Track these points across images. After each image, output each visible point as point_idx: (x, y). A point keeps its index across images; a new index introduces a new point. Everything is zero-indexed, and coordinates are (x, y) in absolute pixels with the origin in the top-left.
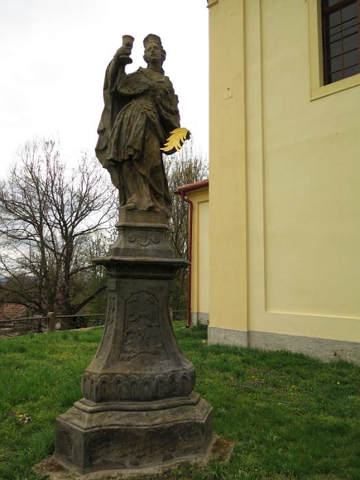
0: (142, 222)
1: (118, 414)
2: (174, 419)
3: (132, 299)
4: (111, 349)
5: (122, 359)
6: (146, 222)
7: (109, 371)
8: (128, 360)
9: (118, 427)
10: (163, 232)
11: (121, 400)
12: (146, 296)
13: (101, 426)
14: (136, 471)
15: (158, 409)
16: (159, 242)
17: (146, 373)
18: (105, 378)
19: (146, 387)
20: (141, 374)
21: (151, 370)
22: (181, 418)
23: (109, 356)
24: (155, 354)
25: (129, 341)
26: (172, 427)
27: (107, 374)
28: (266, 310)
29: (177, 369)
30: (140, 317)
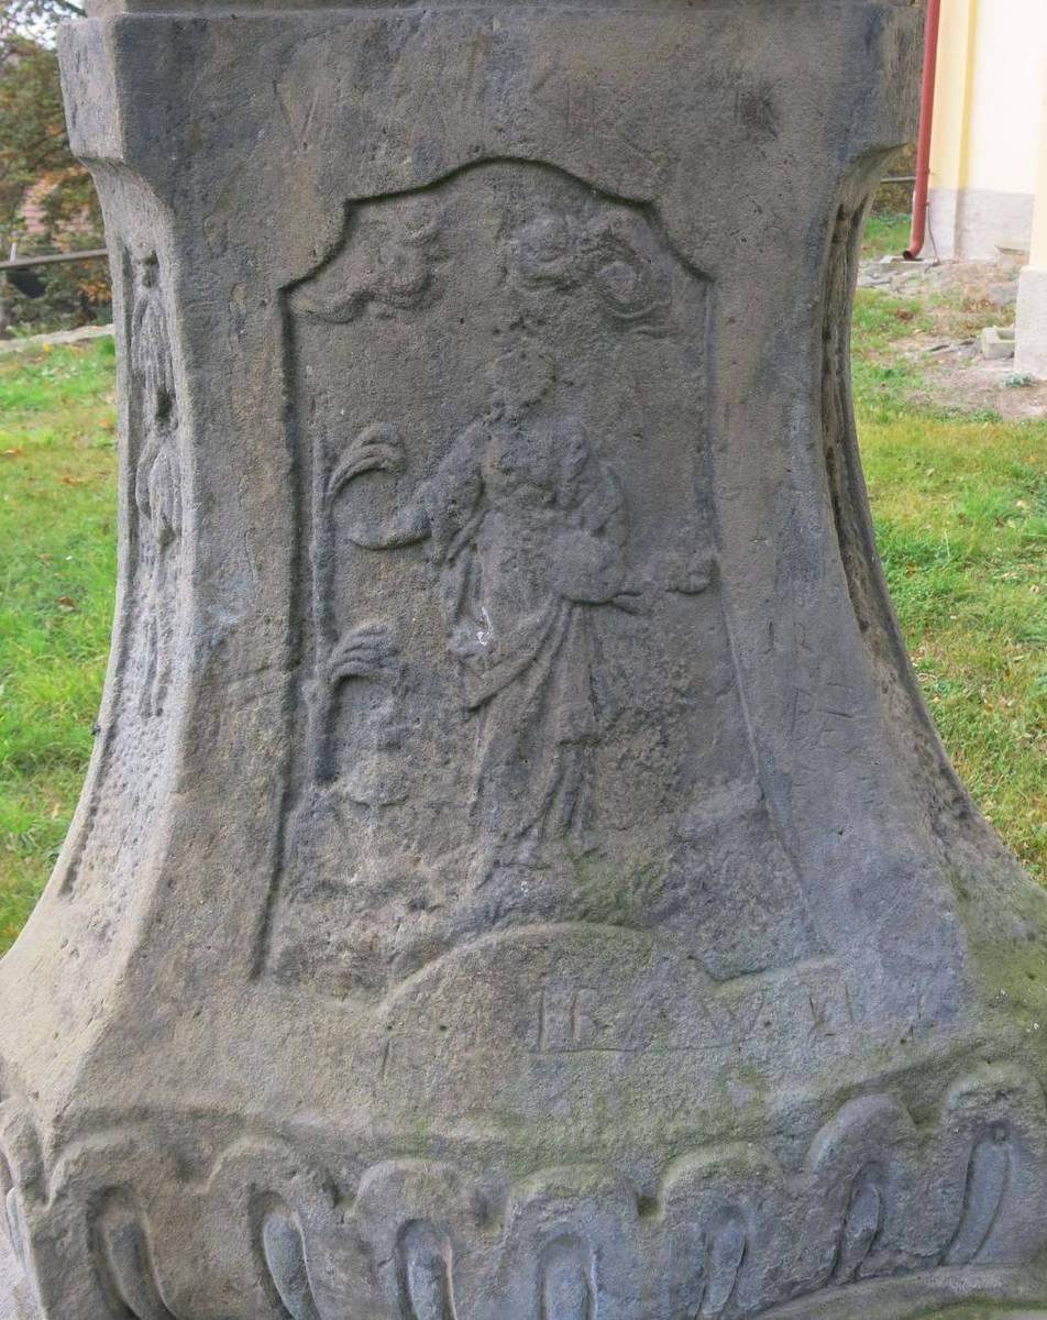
3: (354, 272)
4: (174, 852)
5: (297, 966)
12: (543, 225)
23: (155, 921)
25: (361, 777)
30: (477, 496)
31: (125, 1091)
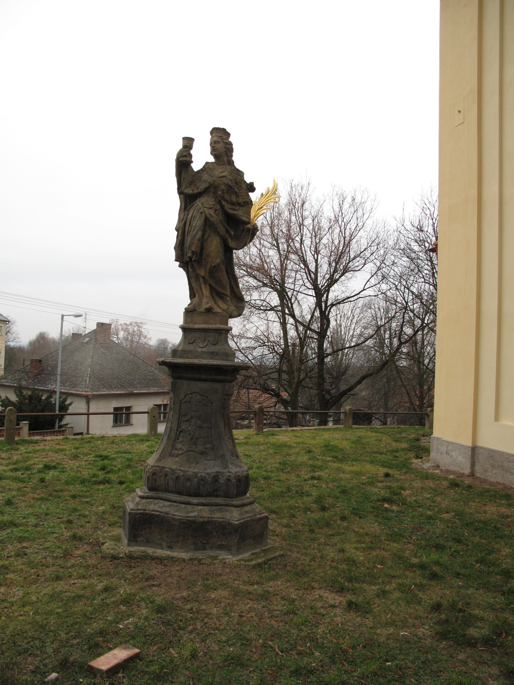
0: (200, 324)
1: (162, 503)
2: (210, 516)
3: (185, 400)
5: (173, 456)
6: (205, 323)
7: (160, 464)
8: (177, 456)
9: (158, 513)
10: (221, 333)
11: (170, 492)
13: (145, 510)
14: (169, 553)
15: (198, 505)
16: (217, 343)
17: (190, 470)
18: (156, 469)
19: (188, 483)
20: (184, 470)
21: (195, 468)
22: (218, 516)
24: (203, 453)
25: (181, 439)
26: (206, 522)
27: (158, 466)
28: (497, 418)
29: (222, 471)
30: (192, 417)
31: (157, 464)
